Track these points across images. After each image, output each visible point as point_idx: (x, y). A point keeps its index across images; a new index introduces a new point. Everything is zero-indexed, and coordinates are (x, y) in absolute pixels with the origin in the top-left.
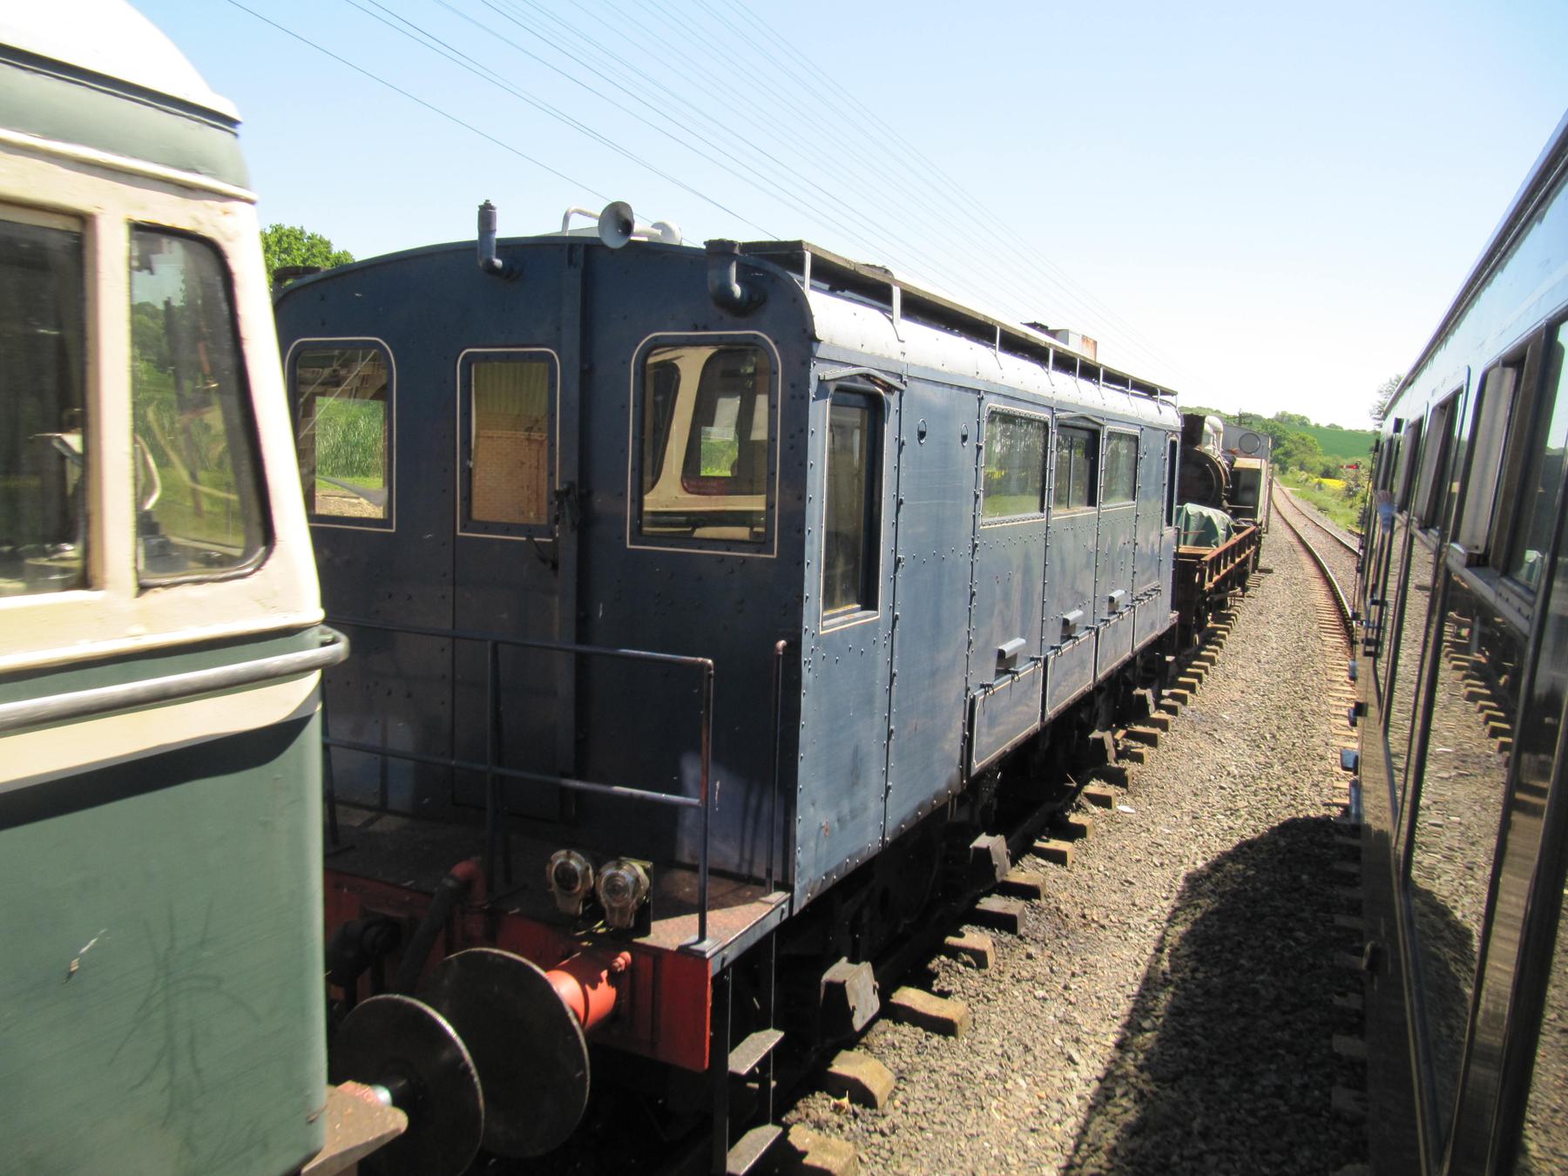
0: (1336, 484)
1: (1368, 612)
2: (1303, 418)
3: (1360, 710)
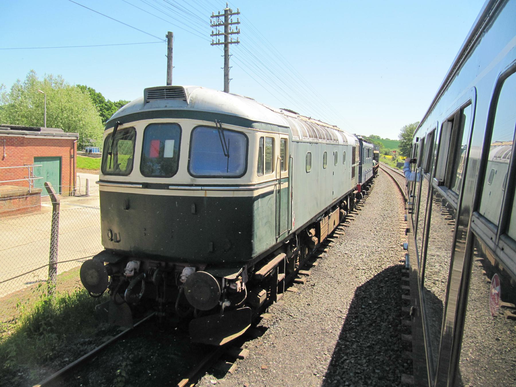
0: (390, 157)
1: (410, 200)
2: (378, 136)
3: (408, 231)
